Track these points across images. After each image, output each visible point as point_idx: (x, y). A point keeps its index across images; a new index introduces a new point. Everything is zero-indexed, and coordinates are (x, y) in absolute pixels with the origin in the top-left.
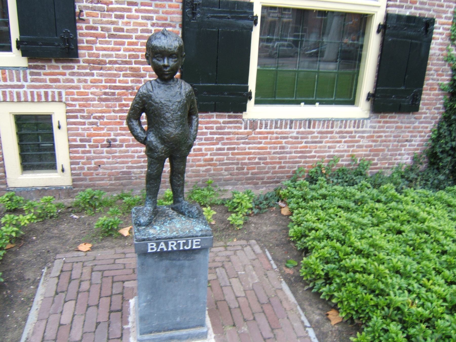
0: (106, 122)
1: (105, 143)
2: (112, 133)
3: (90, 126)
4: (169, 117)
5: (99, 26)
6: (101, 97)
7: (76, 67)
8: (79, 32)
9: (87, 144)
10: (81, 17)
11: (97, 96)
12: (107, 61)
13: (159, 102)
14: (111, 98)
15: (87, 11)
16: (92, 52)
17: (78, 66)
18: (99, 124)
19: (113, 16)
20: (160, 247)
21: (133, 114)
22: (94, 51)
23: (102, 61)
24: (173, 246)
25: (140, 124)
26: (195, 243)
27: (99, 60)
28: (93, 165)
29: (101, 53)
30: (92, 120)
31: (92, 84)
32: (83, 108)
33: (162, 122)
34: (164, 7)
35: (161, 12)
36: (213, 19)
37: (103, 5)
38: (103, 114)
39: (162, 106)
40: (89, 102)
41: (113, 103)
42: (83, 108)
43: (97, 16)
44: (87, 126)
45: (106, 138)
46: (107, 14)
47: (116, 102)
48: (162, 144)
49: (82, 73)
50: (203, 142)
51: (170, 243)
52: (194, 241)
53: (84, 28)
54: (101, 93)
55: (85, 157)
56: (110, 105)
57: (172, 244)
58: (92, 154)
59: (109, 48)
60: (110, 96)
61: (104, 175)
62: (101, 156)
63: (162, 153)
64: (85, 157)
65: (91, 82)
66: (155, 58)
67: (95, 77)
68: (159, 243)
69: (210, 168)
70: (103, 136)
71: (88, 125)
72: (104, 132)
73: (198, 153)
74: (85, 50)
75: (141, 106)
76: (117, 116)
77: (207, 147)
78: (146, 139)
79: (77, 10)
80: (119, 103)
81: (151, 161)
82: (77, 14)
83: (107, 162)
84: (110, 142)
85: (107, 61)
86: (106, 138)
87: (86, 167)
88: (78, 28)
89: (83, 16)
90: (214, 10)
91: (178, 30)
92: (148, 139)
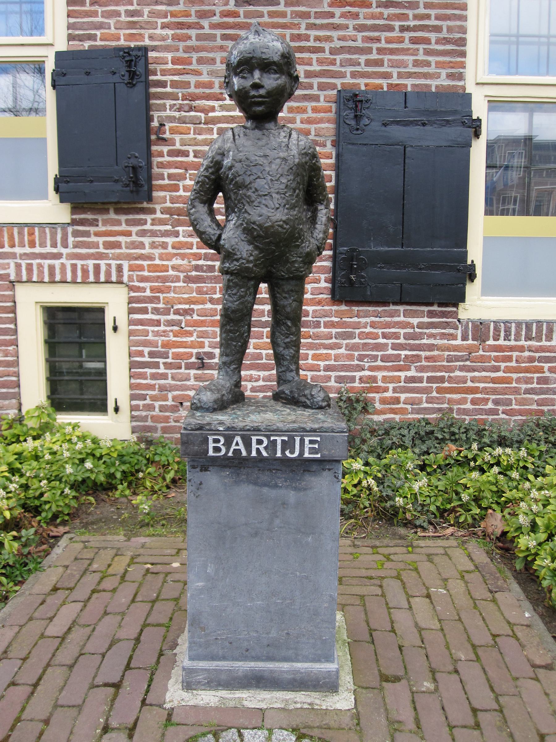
0: (196, 320)
1: (193, 360)
2: (206, 341)
3: (168, 329)
5: (191, 149)
6: (189, 274)
7: (149, 221)
8: (156, 160)
9: (161, 361)
15: (171, 125)
16: (178, 194)
17: (153, 220)
18: (183, 325)
20: (233, 447)
24: (261, 448)
25: (212, 212)
26: (307, 445)
28: (170, 403)
30: (172, 317)
31: (175, 251)
32: (158, 294)
33: (249, 197)
37: (199, 114)
38: (192, 306)
40: (167, 284)
41: (209, 285)
42: (158, 294)
44: (162, 328)
45: (195, 351)
47: (216, 283)
48: (250, 243)
50: (379, 363)
51: (254, 439)
52: (307, 440)
53: (165, 153)
55: (157, 386)
56: (205, 289)
57: (260, 442)
58: (170, 381)
60: (205, 272)
62: (185, 385)
63: (248, 262)
64: (157, 386)
65: (173, 248)
67: (181, 239)
70: (190, 347)
71: (164, 325)
72: (192, 339)
75: (212, 173)
77: (386, 373)
79: (155, 124)
81: (229, 280)
84: (202, 359)
86: (195, 351)
87: (157, 404)
89: (165, 133)
91: (330, 151)
92: (223, 237)
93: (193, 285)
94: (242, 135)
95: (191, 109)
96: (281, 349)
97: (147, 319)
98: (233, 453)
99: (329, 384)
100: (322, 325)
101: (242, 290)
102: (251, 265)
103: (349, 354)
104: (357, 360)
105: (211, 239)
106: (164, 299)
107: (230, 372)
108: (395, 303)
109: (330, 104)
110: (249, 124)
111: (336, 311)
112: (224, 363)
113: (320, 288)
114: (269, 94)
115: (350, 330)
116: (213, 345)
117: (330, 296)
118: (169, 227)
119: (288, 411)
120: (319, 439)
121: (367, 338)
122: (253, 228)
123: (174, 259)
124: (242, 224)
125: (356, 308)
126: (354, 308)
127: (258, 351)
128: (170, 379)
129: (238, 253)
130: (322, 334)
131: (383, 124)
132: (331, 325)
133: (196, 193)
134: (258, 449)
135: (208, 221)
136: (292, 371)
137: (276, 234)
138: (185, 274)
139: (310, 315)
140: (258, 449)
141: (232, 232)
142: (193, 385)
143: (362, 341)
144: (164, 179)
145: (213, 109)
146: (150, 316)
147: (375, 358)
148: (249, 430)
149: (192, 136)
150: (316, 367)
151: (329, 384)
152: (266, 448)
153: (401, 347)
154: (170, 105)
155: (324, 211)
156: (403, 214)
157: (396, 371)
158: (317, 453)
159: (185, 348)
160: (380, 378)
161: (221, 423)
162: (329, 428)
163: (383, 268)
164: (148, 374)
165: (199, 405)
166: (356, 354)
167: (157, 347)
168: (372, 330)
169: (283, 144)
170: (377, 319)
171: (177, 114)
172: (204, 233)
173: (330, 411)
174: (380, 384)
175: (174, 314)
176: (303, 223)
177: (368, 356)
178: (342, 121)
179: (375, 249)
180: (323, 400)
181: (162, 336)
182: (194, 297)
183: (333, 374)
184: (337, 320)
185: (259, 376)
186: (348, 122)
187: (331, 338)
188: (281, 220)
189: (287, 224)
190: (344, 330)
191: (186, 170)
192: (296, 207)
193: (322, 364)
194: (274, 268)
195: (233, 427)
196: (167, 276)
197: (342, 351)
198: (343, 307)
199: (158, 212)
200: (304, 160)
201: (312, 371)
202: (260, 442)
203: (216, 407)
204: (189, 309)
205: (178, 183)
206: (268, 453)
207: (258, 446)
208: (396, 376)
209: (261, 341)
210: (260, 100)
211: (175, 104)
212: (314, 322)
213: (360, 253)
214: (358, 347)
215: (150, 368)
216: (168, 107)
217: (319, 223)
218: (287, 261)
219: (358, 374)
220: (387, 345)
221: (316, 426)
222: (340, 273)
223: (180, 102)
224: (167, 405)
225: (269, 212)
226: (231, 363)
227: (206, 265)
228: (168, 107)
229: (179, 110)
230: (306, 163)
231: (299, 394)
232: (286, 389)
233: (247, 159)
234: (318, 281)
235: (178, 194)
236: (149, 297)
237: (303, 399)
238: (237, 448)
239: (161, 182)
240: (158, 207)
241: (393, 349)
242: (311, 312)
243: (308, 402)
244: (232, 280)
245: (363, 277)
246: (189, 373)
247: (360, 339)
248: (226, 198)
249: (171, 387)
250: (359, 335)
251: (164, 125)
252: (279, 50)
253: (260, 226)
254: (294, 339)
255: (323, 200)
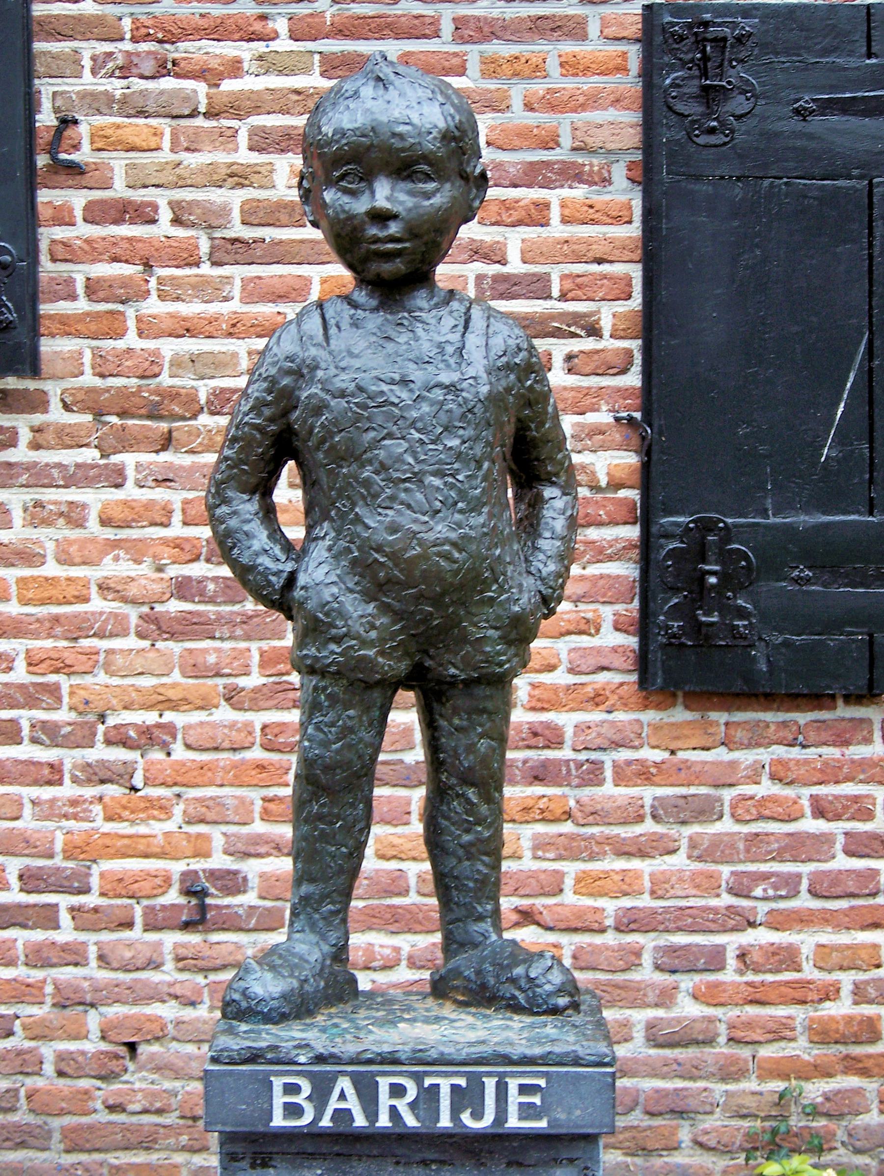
0: (183, 764)
1: (173, 897)
2: (217, 835)
3: (89, 792)
4: (399, 459)
5: (162, 199)
6: (159, 608)
7: (25, 436)
8: (48, 234)
9: (64, 901)
10: (63, 156)
11: (134, 602)
12: (203, 398)
13: (352, 387)
14: (220, 616)
15: (99, 120)
16: (121, 344)
17: (37, 430)
18: (138, 781)
19: (243, 138)
20: (334, 1104)
21: (236, 463)
22: (131, 340)
23: (173, 395)
24: (402, 1105)
25: (269, 512)
26: (514, 1098)
27: (158, 392)
28: (92, 1045)
29: (169, 347)
30: (100, 753)
31: (110, 534)
32: (53, 678)
33: (367, 483)
34: (538, 70)
35: (517, 103)
36: (835, 119)
37: (188, 84)
38: (169, 716)
39: (364, 407)
40: (85, 643)
41: (227, 645)
42: (53, 678)
43: (153, 143)
44: (67, 790)
45: (177, 867)
46: (210, 131)
47: (248, 638)
48: (369, 597)
49: (59, 465)
50: (804, 902)
51: (384, 1083)
52: (513, 1085)
53: (79, 214)
54: (157, 588)
55: (49, 989)
56: (212, 659)
57: (397, 1091)
58: (93, 971)
59: (212, 320)
60: (212, 601)
61: (160, 1112)
62: (146, 983)
63: (365, 643)
64: (49, 989)
65: (105, 522)
66: (331, 183)
67: (130, 491)
68: (332, 1079)
69: (858, 1092)
70: (161, 855)
71: (75, 780)
72: (170, 826)
73: (770, 978)
74: (78, 335)
75: (271, 420)
76: (248, 728)
77: (828, 937)
78: (291, 579)
79: (46, 118)
80: (265, 645)
81: (316, 688)
82: (44, 138)
83: (179, 1023)
84: (202, 894)
85: (203, 398)
86: (177, 867)
87: (48, 1051)
88: (44, 213)
89: (76, 147)
90: (835, 68)
91: (623, 198)
92: (302, 579)
93: (171, 644)
94: (345, 324)
95: (164, 68)
96: (453, 861)
97: (17, 761)
98: (332, 1119)
99: (634, 976)
100: (608, 773)
101: (351, 712)
102: (371, 653)
103: (701, 873)
104: (731, 891)
105: (270, 583)
106: (72, 694)
107: (321, 924)
108: (852, 699)
109: (621, 47)
110: (361, 296)
111: (656, 728)
112: (305, 900)
113: (598, 651)
114: (412, 232)
115: (703, 790)
116: (240, 846)
117: (634, 677)
118: (90, 455)
119: (470, 1019)
120: (542, 1083)
121: (761, 817)
122: (376, 560)
123: (108, 559)
124: (349, 550)
125: (720, 717)
126: (714, 715)
127: (393, 865)
128: (94, 963)
129: (340, 623)
130: (608, 806)
131: (797, 112)
132: (639, 774)
133: (229, 467)
134: (393, 1109)
135: (261, 538)
136: (481, 918)
137: (433, 576)
138: (145, 609)
139: (568, 742)
140: (393, 1109)
141: (325, 568)
142: (171, 985)
143: (745, 829)
144: (73, 297)
145: (235, 68)
146: (25, 751)
147: (791, 884)
148: (370, 1062)
149: (166, 155)
150: (590, 917)
151: (634, 976)
152: (413, 1106)
153: (876, 845)
154: (94, 58)
155: (559, 504)
156: (871, 403)
157: (864, 927)
158: (538, 1117)
159: (146, 856)
160: (807, 950)
161: (305, 1046)
162: (567, 1054)
163: (808, 581)
164: (20, 944)
165: (244, 1004)
166: (726, 870)
167: (51, 856)
168: (777, 789)
169: (450, 349)
170: (795, 753)
171: (116, 86)
172: (252, 568)
173: (577, 1019)
174: (809, 972)
175: (109, 742)
176: (503, 542)
177: (765, 877)
178: (659, 104)
179: (778, 520)
180: (560, 991)
181: (66, 816)
182: (174, 686)
183: (648, 942)
184: (658, 755)
185: (397, 950)
186: (680, 107)
187: (640, 819)
188: (447, 541)
189: (460, 551)
190: (683, 791)
191: (148, 266)
192: (485, 504)
193: (610, 906)
194: (431, 658)
195: (332, 1055)
196: (84, 618)
197: (679, 861)
198: (680, 715)
199: (55, 404)
200: (504, 383)
201: (576, 930)
202: (397, 1091)
203: (286, 1010)
204: (159, 726)
205: (120, 307)
206: (418, 1118)
207: (394, 1102)
208: (863, 946)
209: (400, 830)
210: (390, 246)
211: (110, 54)
212: (579, 765)
213: (728, 534)
214: (733, 846)
215: (24, 926)
216: (87, 63)
217: (547, 534)
218: (464, 639)
219: (732, 942)
220: (827, 839)
221: (537, 1051)
222: (666, 601)
223: (127, 46)
224: (83, 1053)
225: (415, 521)
226: (324, 897)
227: (215, 579)
228: (87, 63)
229: (125, 71)
230: (508, 390)
231: (497, 976)
232: (466, 962)
233: (360, 389)
234: (589, 627)
235: (121, 344)
236: (22, 687)
237: (509, 990)
238: (342, 1105)
239: (63, 307)
240: (54, 389)
241: (850, 853)
242: (569, 732)
243: (521, 997)
244: (325, 689)
245: (742, 613)
246: (160, 943)
247: (738, 821)
248: (309, 483)
249: (97, 990)
250: (733, 807)
251: (76, 122)
252: (436, 127)
253: (394, 556)
254: (486, 834)
255: (557, 475)
